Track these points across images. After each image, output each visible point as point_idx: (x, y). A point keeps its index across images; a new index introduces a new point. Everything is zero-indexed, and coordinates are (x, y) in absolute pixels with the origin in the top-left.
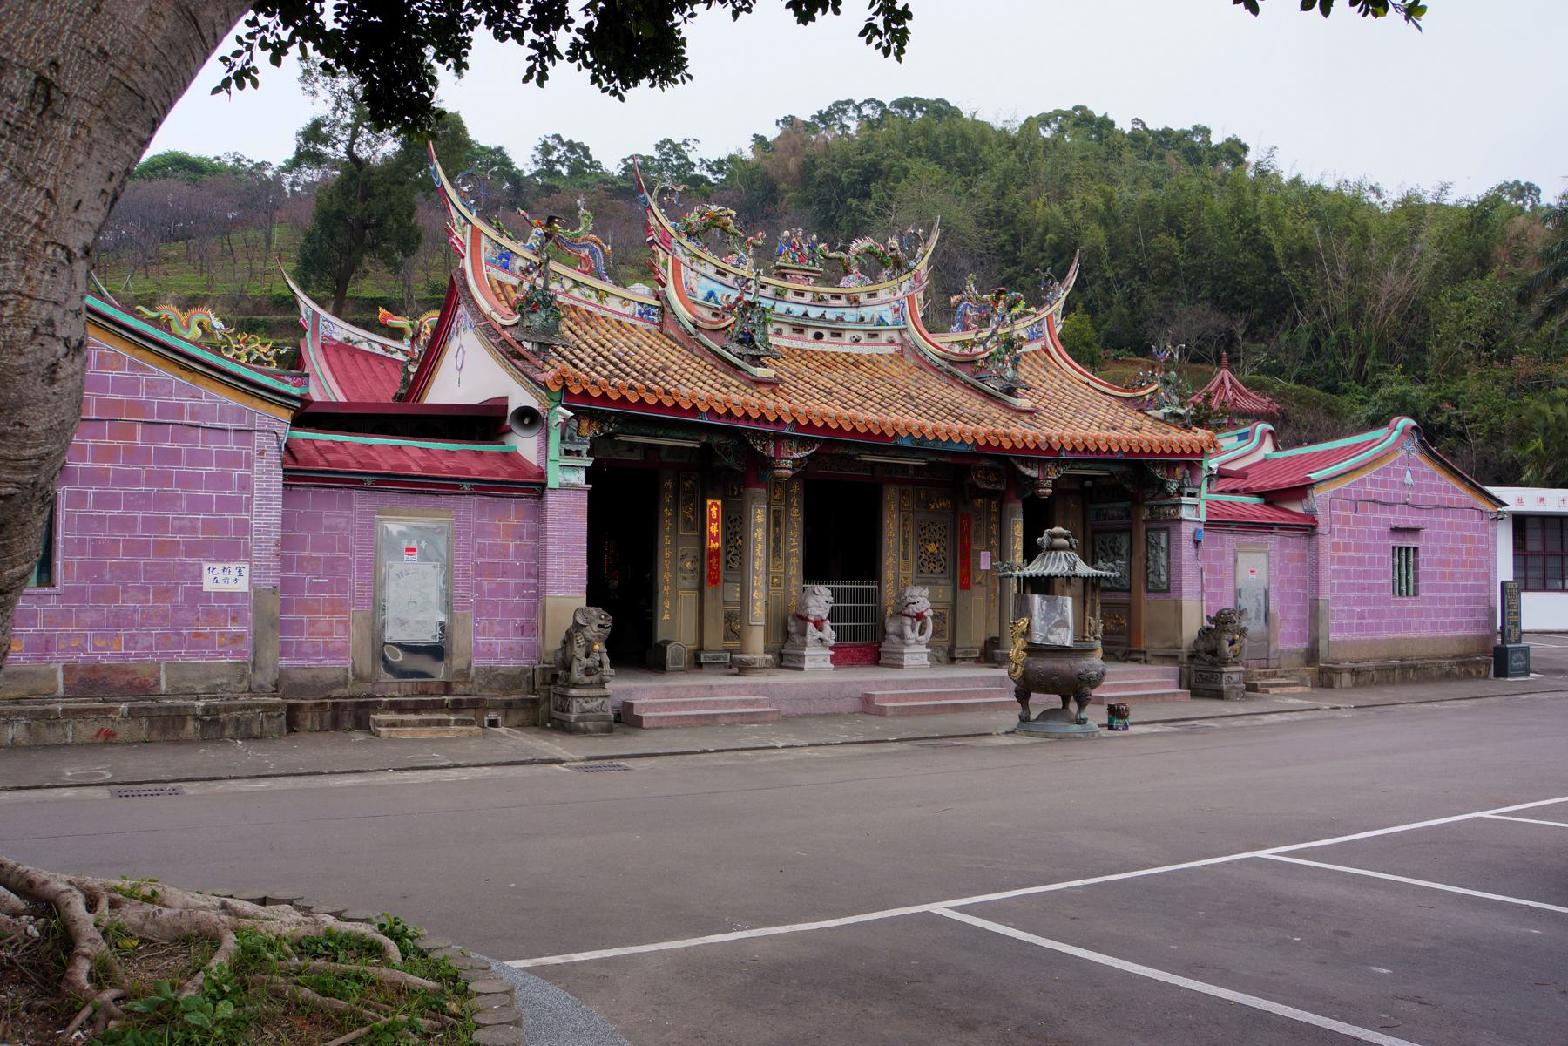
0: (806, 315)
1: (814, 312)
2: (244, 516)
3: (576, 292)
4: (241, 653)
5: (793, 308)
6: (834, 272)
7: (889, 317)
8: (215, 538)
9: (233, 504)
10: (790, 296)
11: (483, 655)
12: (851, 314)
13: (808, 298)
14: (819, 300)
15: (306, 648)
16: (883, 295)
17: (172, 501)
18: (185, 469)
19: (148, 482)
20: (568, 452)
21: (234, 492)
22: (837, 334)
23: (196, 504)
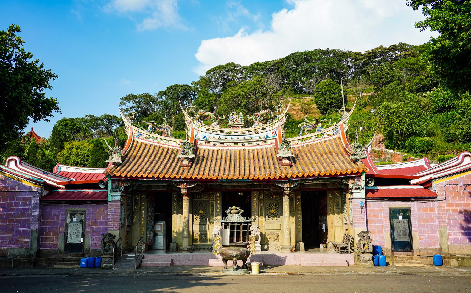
0: (226, 138)
1: (241, 138)
2: (30, 212)
3: (162, 142)
4: (28, 246)
5: (233, 137)
6: (248, 124)
7: (271, 135)
8: (23, 218)
9: (27, 210)
10: (233, 133)
11: (93, 246)
12: (255, 137)
13: (239, 133)
14: (243, 134)
15: (47, 245)
16: (267, 128)
17: (13, 210)
18: (16, 202)
19: (8, 206)
20: (114, 191)
21: (27, 207)
22: (250, 143)
23: (18, 210)
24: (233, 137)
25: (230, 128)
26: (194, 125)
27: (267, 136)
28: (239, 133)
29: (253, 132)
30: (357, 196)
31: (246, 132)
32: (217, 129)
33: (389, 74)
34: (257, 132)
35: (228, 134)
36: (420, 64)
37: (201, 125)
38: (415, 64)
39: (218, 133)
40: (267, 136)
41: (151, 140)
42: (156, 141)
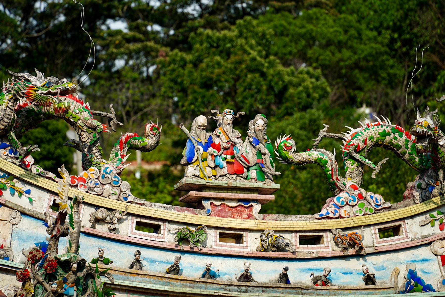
5: (217, 264)
6: (306, 191)
10: (212, 240)
13: (252, 243)
14: (274, 249)
16: (413, 230)
24: (217, 264)
25: (196, 204)
27: (412, 275)
28: (252, 243)
29: (328, 246)
31: (293, 239)
32: (120, 206)
33: (263, 75)
34: (353, 248)
35: (188, 241)
36: (365, 49)
37: (17, 171)
38: (340, 45)
39: (128, 229)
40: (412, 275)
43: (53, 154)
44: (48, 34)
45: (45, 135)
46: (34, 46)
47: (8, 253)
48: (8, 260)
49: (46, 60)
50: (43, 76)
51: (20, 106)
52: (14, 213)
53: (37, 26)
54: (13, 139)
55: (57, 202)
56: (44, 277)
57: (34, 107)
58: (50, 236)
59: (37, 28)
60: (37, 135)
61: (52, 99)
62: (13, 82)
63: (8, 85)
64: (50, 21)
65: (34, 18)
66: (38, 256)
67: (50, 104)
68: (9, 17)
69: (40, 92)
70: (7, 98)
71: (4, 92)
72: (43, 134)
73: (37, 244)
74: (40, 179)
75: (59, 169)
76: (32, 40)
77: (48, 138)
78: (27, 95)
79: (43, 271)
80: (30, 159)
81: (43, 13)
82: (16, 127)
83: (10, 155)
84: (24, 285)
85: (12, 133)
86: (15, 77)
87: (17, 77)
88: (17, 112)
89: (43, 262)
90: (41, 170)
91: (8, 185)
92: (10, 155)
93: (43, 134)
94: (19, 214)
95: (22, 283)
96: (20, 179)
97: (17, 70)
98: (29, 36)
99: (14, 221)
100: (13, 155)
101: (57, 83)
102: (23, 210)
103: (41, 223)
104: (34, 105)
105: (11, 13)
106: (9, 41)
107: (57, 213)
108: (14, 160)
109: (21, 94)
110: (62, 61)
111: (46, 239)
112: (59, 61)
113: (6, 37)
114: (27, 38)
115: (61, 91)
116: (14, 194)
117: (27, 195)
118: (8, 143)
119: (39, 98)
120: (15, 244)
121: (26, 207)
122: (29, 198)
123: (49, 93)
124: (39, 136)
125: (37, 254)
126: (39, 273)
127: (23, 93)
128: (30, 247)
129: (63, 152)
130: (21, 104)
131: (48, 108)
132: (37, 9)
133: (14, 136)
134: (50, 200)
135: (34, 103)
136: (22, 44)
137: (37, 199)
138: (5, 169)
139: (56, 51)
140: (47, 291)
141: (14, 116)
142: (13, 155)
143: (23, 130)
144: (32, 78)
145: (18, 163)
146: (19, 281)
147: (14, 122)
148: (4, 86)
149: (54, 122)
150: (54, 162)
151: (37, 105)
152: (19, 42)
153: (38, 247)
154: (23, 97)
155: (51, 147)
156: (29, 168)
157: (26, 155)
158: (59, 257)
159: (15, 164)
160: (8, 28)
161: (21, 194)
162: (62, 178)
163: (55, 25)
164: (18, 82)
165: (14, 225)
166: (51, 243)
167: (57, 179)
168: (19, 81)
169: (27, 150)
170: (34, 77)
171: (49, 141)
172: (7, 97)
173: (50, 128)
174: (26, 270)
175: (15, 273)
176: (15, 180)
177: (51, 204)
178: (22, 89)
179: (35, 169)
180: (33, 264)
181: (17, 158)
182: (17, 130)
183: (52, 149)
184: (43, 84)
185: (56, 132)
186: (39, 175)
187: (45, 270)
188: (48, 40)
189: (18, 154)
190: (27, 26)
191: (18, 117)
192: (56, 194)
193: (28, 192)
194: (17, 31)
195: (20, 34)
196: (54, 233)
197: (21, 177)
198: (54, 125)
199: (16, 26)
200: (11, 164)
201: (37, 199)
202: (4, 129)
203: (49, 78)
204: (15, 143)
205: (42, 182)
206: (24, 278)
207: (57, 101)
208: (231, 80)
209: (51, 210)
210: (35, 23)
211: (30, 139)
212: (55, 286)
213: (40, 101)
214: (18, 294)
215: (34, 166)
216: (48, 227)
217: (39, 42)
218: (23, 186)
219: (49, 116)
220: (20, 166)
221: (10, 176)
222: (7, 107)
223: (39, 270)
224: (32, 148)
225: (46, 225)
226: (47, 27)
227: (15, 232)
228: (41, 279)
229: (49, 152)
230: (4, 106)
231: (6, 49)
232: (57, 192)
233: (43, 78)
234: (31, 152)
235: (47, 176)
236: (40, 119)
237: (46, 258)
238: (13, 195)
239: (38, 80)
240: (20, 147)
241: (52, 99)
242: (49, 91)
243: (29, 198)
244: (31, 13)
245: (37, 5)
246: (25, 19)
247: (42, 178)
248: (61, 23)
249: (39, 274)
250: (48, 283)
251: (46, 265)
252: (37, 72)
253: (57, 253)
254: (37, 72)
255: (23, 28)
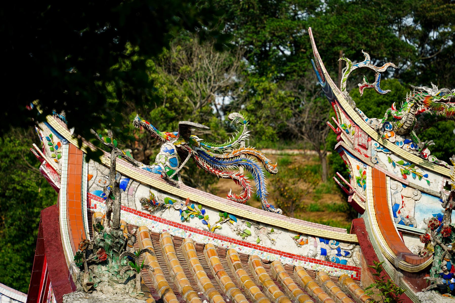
3: (227, 230)
26: (383, 157)
30: (9, 262)
37: (417, 160)
41: (171, 214)
42: (195, 222)
43: (442, 147)
44: (439, 56)
45: (436, 133)
46: (428, 66)
47: (413, 222)
48: (413, 227)
49: (437, 75)
50: (437, 88)
51: (419, 112)
52: (416, 192)
53: (430, 50)
54: (414, 136)
55: (449, 183)
56: (441, 240)
57: (430, 112)
58: (444, 209)
59: (431, 52)
60: (430, 132)
61: (444, 105)
62: (414, 94)
63: (411, 96)
64: (441, 46)
65: (428, 44)
66: (436, 224)
67: (443, 108)
68: (409, 45)
69: (435, 100)
70: (410, 106)
71: (407, 101)
72: (434, 132)
73: (434, 215)
74: (436, 166)
75: (450, 159)
76: (426, 61)
77: (438, 135)
78: (425, 103)
79: (440, 235)
80: (427, 152)
81: (435, 40)
82: (416, 128)
83: (412, 148)
84: (426, 245)
85: (413, 132)
86: (416, 90)
87: (418, 90)
88: (417, 116)
89: (440, 229)
90: (436, 159)
91: (411, 171)
92: (412, 148)
93: (434, 132)
94: (420, 192)
95: (424, 244)
96: (419, 166)
97: (415, 84)
98: (424, 58)
99: (416, 198)
100: (414, 149)
101: (448, 93)
102: (422, 189)
103: (437, 200)
104: (430, 110)
105: (411, 42)
106: (409, 63)
107: (450, 192)
108: (415, 152)
109: (420, 102)
110: (450, 76)
111: (442, 211)
112: (447, 76)
113: (407, 60)
114: (422, 60)
115: (451, 99)
116: (415, 178)
117: (425, 178)
118: (410, 140)
119: (434, 105)
120: (418, 215)
121: (425, 187)
122: (427, 180)
123: (442, 101)
124: (432, 133)
125: (435, 223)
126: (438, 237)
127: (422, 101)
128: (429, 218)
129: (450, 145)
130: (420, 110)
131: (441, 112)
132: (431, 37)
133: (415, 134)
134: (443, 182)
135: (430, 109)
136: (419, 65)
137: (433, 182)
138: (408, 159)
139: (445, 68)
140: (444, 250)
141: (415, 119)
142: (414, 149)
143: (421, 130)
144: (429, 90)
145: (418, 155)
146: (422, 242)
147: (415, 123)
148: (407, 97)
149: (444, 123)
150: (444, 153)
151: (433, 110)
152: (416, 63)
153: (435, 218)
154: (421, 104)
155: (441, 142)
156: (426, 158)
157: (424, 148)
158: (452, 225)
159: (416, 155)
160: (409, 53)
161: (421, 178)
162: (453, 165)
163: (445, 49)
164: (417, 93)
165: (416, 200)
166: (446, 214)
167: (448, 166)
168: (419, 93)
169: (425, 144)
170: (430, 89)
171: (439, 137)
172: (410, 105)
173: (440, 127)
174: (427, 235)
175: (419, 236)
176: (416, 167)
177: (445, 185)
178: (421, 98)
179: (431, 159)
180: (432, 230)
181: (417, 151)
182: (417, 129)
183: (442, 144)
184: (437, 94)
185: (445, 130)
186: (434, 163)
187: (442, 235)
188: (438, 60)
189: (418, 148)
190: (423, 51)
191: (417, 120)
192: (449, 178)
193: (426, 176)
194: (415, 55)
195: (417, 57)
196: (448, 207)
197: (421, 165)
198: (443, 124)
199: (414, 51)
200: (413, 155)
201: (433, 182)
202: (407, 129)
203: (442, 89)
204: (416, 139)
205: (437, 169)
206: (426, 240)
207: (448, 107)
208: (29, 132)
209: (444, 190)
210: (429, 48)
211: (424, 136)
212: (450, 247)
213: (434, 107)
214: (422, 252)
215: (430, 156)
216: (443, 202)
217: (432, 63)
218: (422, 171)
219: (442, 118)
220: (420, 156)
221: (412, 164)
222: (410, 112)
223: (437, 234)
224: (429, 143)
225: (441, 201)
226: (438, 50)
227: (417, 206)
228: (439, 241)
229: (439, 146)
230: (407, 112)
231: (406, 69)
232: (449, 176)
233: (437, 90)
234: (428, 146)
235: (440, 164)
236: (435, 121)
237: (442, 226)
238: (415, 178)
239: (433, 92)
240: (419, 142)
241: (444, 105)
242: (442, 99)
243: (427, 180)
244: (427, 41)
245: (431, 34)
246: (422, 45)
247: (437, 166)
248: (450, 46)
249: (438, 238)
250: (445, 245)
251: (442, 231)
252: (433, 85)
253: (451, 222)
254: (433, 85)
255: (419, 53)
